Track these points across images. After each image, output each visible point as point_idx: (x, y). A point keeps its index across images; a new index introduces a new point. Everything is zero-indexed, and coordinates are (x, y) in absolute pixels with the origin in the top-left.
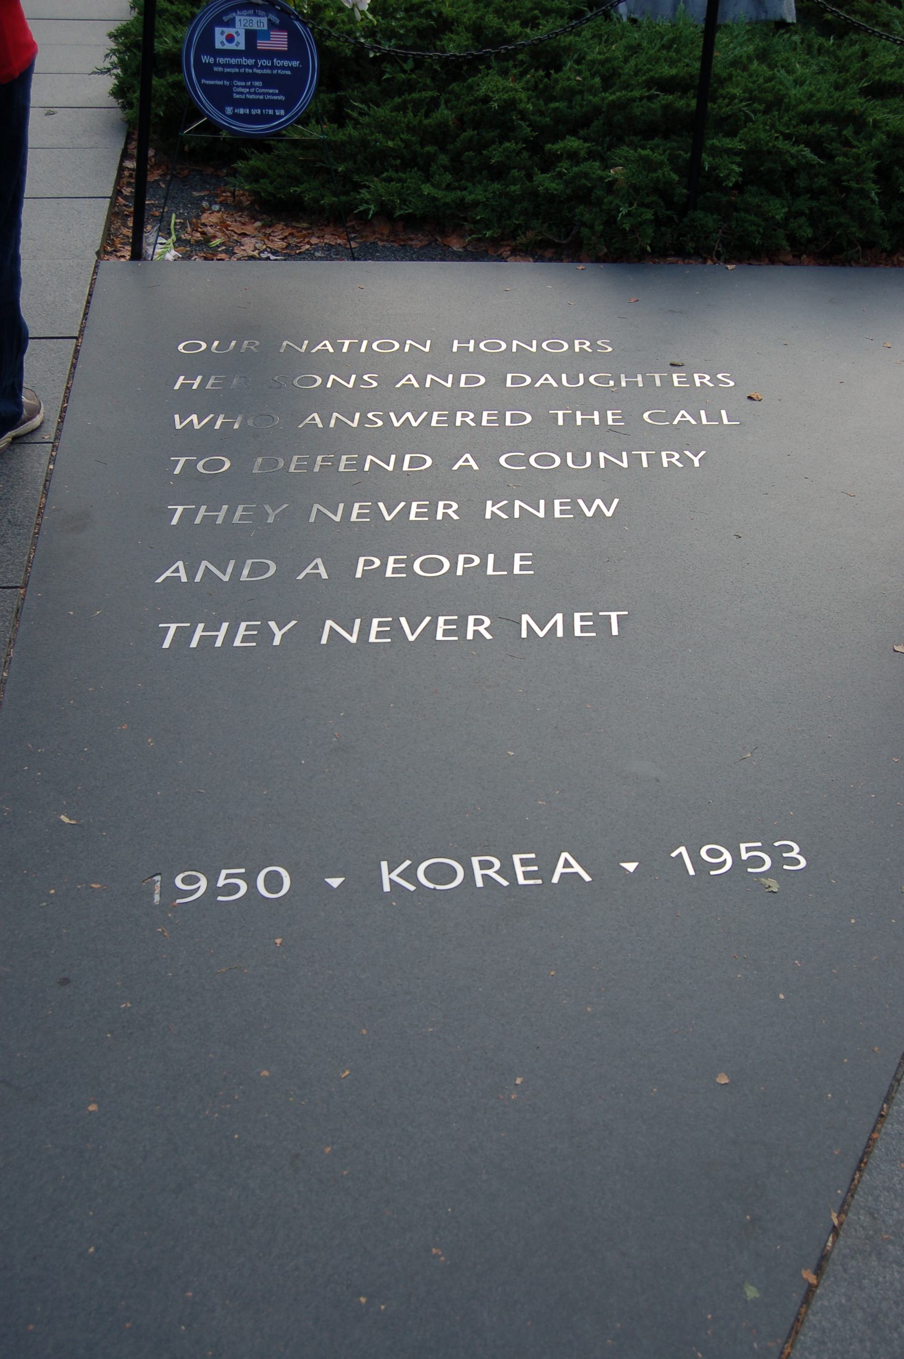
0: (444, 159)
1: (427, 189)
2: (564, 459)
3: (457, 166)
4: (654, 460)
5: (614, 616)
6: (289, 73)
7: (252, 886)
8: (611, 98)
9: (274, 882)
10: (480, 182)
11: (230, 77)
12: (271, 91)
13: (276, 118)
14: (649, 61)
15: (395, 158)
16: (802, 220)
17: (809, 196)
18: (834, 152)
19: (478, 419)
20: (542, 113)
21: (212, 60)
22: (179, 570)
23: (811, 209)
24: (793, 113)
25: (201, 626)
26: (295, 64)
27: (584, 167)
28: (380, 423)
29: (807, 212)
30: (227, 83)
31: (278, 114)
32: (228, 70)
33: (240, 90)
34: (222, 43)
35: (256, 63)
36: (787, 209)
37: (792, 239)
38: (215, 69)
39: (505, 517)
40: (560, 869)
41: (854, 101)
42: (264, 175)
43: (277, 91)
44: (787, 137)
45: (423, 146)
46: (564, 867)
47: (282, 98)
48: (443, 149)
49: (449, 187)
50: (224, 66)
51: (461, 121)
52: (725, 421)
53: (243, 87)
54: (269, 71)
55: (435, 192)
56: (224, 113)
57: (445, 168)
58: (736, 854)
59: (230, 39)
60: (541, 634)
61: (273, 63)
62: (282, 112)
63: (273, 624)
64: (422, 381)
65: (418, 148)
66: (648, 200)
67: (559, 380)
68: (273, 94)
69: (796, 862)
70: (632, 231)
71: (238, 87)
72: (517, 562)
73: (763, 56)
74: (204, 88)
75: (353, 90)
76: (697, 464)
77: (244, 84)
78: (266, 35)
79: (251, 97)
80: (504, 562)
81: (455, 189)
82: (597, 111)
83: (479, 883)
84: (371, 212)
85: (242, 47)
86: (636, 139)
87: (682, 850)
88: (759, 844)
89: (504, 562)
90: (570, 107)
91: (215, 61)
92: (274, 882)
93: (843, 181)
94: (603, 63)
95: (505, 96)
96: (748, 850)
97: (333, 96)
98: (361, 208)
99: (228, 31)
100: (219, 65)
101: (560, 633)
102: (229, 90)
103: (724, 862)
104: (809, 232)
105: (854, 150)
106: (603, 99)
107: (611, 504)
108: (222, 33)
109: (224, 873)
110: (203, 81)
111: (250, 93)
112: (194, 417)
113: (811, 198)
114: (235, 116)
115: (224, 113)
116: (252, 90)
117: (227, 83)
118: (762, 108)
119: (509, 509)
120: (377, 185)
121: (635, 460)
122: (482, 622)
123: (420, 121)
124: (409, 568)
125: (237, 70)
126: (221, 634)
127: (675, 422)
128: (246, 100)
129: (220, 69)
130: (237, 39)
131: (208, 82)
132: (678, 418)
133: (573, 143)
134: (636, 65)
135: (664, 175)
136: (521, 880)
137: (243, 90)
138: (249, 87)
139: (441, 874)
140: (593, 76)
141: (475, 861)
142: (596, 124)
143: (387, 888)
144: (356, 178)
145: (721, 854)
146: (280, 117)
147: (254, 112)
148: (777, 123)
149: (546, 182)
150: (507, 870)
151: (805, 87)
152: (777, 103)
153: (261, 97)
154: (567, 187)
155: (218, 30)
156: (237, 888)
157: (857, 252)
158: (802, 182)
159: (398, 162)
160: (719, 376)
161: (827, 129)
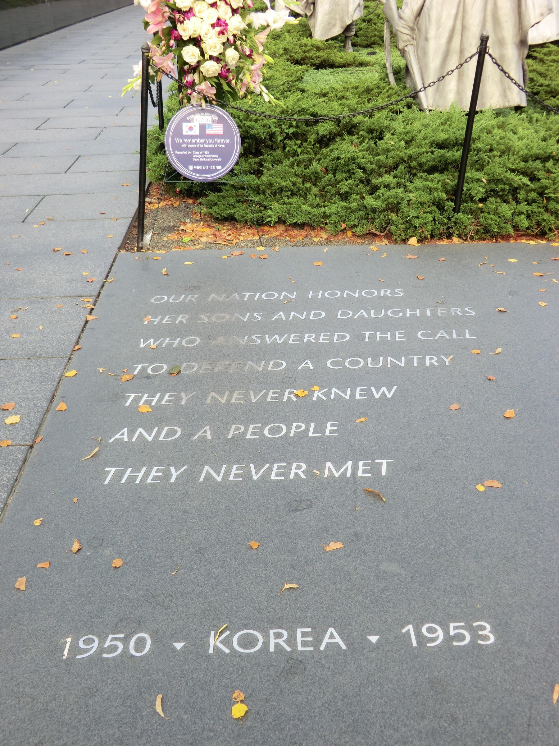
0: (315, 190)
1: (305, 207)
2: (365, 362)
3: (323, 194)
4: (422, 362)
5: (384, 462)
6: (223, 146)
7: (126, 647)
8: (409, 153)
9: (140, 644)
10: (334, 203)
11: (191, 149)
12: (214, 156)
13: (216, 170)
14: (433, 131)
15: (287, 191)
16: (523, 217)
17: (526, 203)
18: (540, 177)
19: (317, 339)
20: (371, 163)
21: (181, 141)
22: (124, 435)
23: (527, 211)
24: (517, 157)
25: (130, 470)
26: (227, 141)
27: (393, 192)
28: (259, 341)
29: (525, 212)
30: (189, 153)
31: (218, 168)
32: (190, 146)
33: (197, 156)
34: (187, 132)
35: (205, 142)
36: (513, 211)
37: (516, 228)
38: (183, 145)
39: (325, 399)
40: (326, 640)
41: (553, 147)
42: (215, 204)
43: (217, 156)
44: (513, 171)
45: (303, 184)
46: (329, 639)
47: (220, 160)
48: (315, 185)
49: (318, 206)
50: (187, 144)
51: (327, 171)
52: (468, 337)
53: (198, 154)
54: (212, 146)
55: (309, 209)
56: (188, 169)
57: (316, 195)
58: (446, 631)
59: (191, 128)
60: (337, 475)
61: (214, 141)
62: (220, 167)
63: (172, 469)
64: (287, 317)
65: (301, 185)
66: (428, 210)
67: (369, 314)
68: (215, 158)
69: (486, 638)
70: (421, 227)
71: (195, 154)
72: (329, 427)
73: (501, 126)
74: (177, 156)
75: (268, 155)
76: (447, 364)
77: (198, 153)
78: (211, 127)
79: (202, 160)
80: (320, 428)
81: (321, 207)
82: (402, 160)
83: (272, 649)
84: (273, 222)
85: (197, 133)
86: (424, 175)
87: (410, 627)
88: (463, 624)
89: (320, 428)
90: (387, 158)
91: (183, 141)
92: (140, 644)
93: (545, 194)
94: (407, 133)
95: (349, 155)
96: (456, 628)
97: (257, 160)
98: (267, 220)
99: (189, 125)
100: (185, 143)
101: (349, 475)
102: (191, 156)
103: (438, 637)
104: (526, 224)
105: (553, 175)
106: (405, 153)
107: (391, 390)
108: (187, 126)
109: (111, 636)
110: (176, 152)
111: (202, 158)
112: (152, 340)
113: (528, 204)
114: (194, 170)
115: (188, 169)
116: (203, 156)
117: (189, 153)
118: (498, 154)
119: (328, 395)
120: (276, 206)
121: (409, 362)
122: (301, 467)
123: (302, 171)
124: (261, 433)
125: (195, 146)
126: (141, 475)
127: (437, 338)
128: (200, 161)
129: (185, 145)
130: (194, 128)
131: (179, 153)
132: (439, 335)
133: (387, 179)
134: (425, 134)
135: (438, 195)
136: (300, 648)
137: (198, 156)
138: (202, 155)
139: (248, 642)
140: (400, 141)
141: (272, 632)
142: (401, 167)
143: (211, 651)
144: (266, 204)
145: (436, 631)
146: (219, 170)
147: (204, 168)
148: (507, 162)
149: (370, 201)
150: (291, 641)
151: (524, 141)
152: (507, 151)
153: (208, 160)
154: (383, 203)
155: (184, 125)
156: (115, 648)
157: (555, 235)
158: (521, 195)
159: (289, 193)
160: (467, 309)
161: (538, 164)
